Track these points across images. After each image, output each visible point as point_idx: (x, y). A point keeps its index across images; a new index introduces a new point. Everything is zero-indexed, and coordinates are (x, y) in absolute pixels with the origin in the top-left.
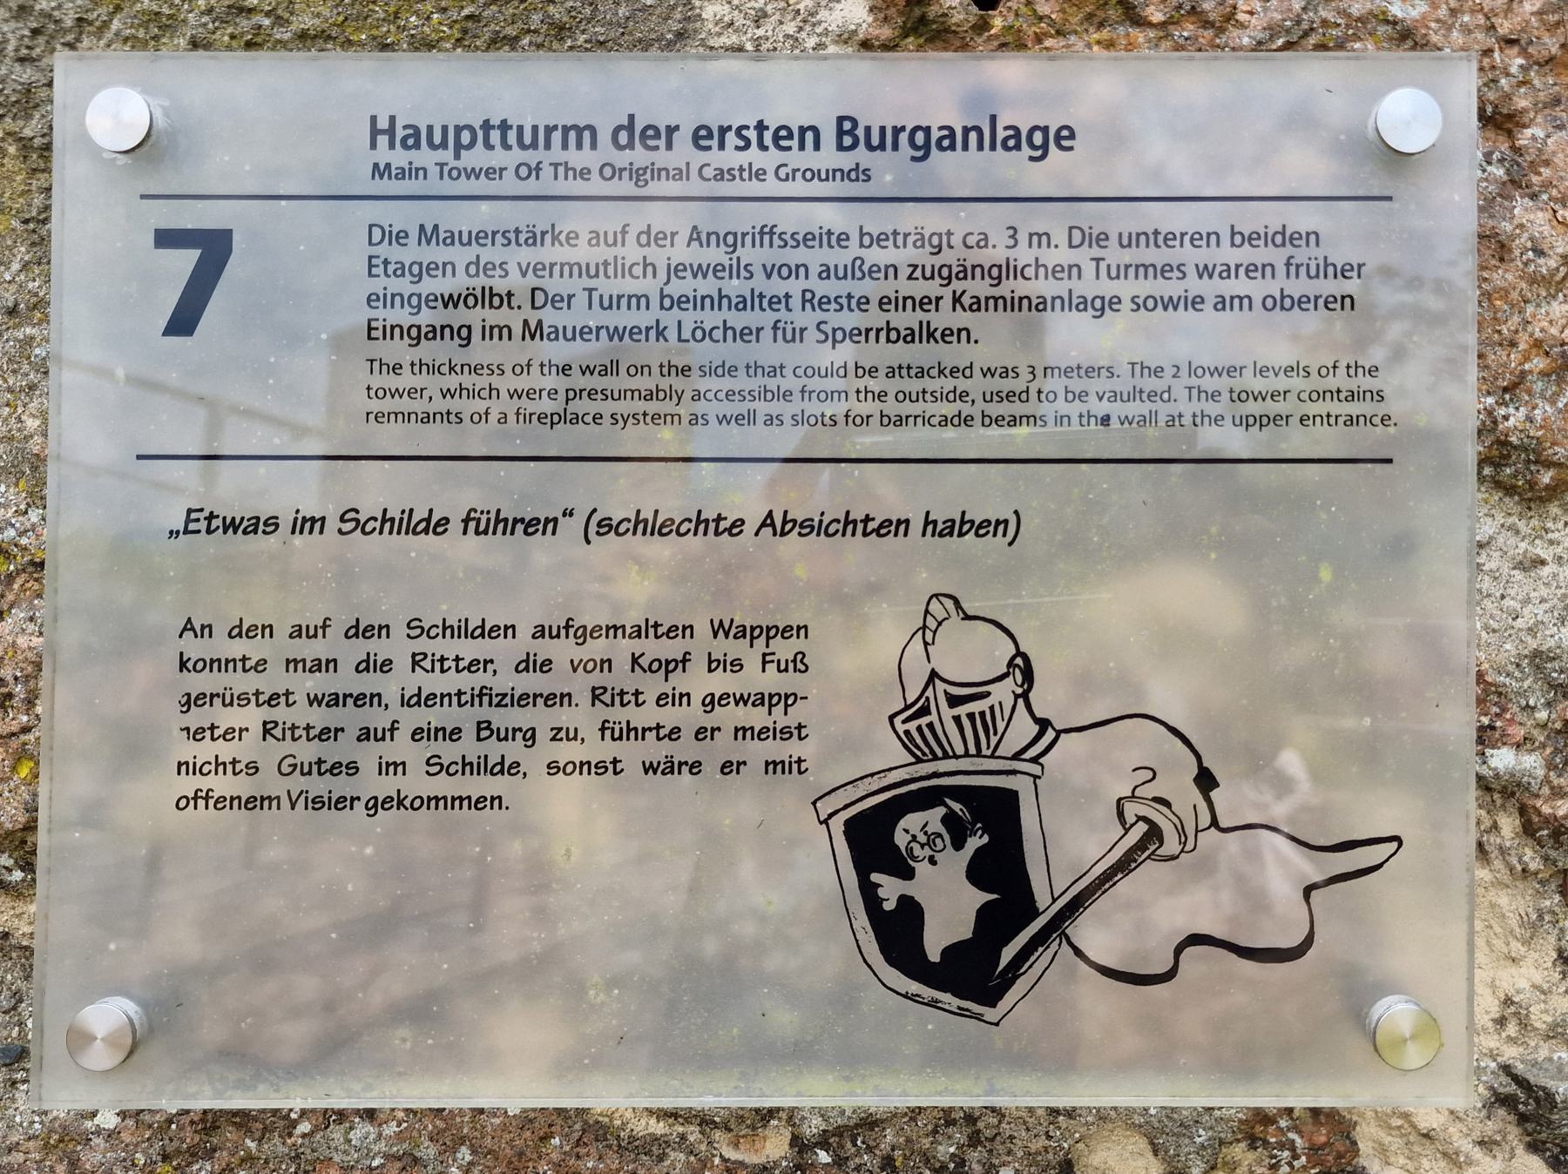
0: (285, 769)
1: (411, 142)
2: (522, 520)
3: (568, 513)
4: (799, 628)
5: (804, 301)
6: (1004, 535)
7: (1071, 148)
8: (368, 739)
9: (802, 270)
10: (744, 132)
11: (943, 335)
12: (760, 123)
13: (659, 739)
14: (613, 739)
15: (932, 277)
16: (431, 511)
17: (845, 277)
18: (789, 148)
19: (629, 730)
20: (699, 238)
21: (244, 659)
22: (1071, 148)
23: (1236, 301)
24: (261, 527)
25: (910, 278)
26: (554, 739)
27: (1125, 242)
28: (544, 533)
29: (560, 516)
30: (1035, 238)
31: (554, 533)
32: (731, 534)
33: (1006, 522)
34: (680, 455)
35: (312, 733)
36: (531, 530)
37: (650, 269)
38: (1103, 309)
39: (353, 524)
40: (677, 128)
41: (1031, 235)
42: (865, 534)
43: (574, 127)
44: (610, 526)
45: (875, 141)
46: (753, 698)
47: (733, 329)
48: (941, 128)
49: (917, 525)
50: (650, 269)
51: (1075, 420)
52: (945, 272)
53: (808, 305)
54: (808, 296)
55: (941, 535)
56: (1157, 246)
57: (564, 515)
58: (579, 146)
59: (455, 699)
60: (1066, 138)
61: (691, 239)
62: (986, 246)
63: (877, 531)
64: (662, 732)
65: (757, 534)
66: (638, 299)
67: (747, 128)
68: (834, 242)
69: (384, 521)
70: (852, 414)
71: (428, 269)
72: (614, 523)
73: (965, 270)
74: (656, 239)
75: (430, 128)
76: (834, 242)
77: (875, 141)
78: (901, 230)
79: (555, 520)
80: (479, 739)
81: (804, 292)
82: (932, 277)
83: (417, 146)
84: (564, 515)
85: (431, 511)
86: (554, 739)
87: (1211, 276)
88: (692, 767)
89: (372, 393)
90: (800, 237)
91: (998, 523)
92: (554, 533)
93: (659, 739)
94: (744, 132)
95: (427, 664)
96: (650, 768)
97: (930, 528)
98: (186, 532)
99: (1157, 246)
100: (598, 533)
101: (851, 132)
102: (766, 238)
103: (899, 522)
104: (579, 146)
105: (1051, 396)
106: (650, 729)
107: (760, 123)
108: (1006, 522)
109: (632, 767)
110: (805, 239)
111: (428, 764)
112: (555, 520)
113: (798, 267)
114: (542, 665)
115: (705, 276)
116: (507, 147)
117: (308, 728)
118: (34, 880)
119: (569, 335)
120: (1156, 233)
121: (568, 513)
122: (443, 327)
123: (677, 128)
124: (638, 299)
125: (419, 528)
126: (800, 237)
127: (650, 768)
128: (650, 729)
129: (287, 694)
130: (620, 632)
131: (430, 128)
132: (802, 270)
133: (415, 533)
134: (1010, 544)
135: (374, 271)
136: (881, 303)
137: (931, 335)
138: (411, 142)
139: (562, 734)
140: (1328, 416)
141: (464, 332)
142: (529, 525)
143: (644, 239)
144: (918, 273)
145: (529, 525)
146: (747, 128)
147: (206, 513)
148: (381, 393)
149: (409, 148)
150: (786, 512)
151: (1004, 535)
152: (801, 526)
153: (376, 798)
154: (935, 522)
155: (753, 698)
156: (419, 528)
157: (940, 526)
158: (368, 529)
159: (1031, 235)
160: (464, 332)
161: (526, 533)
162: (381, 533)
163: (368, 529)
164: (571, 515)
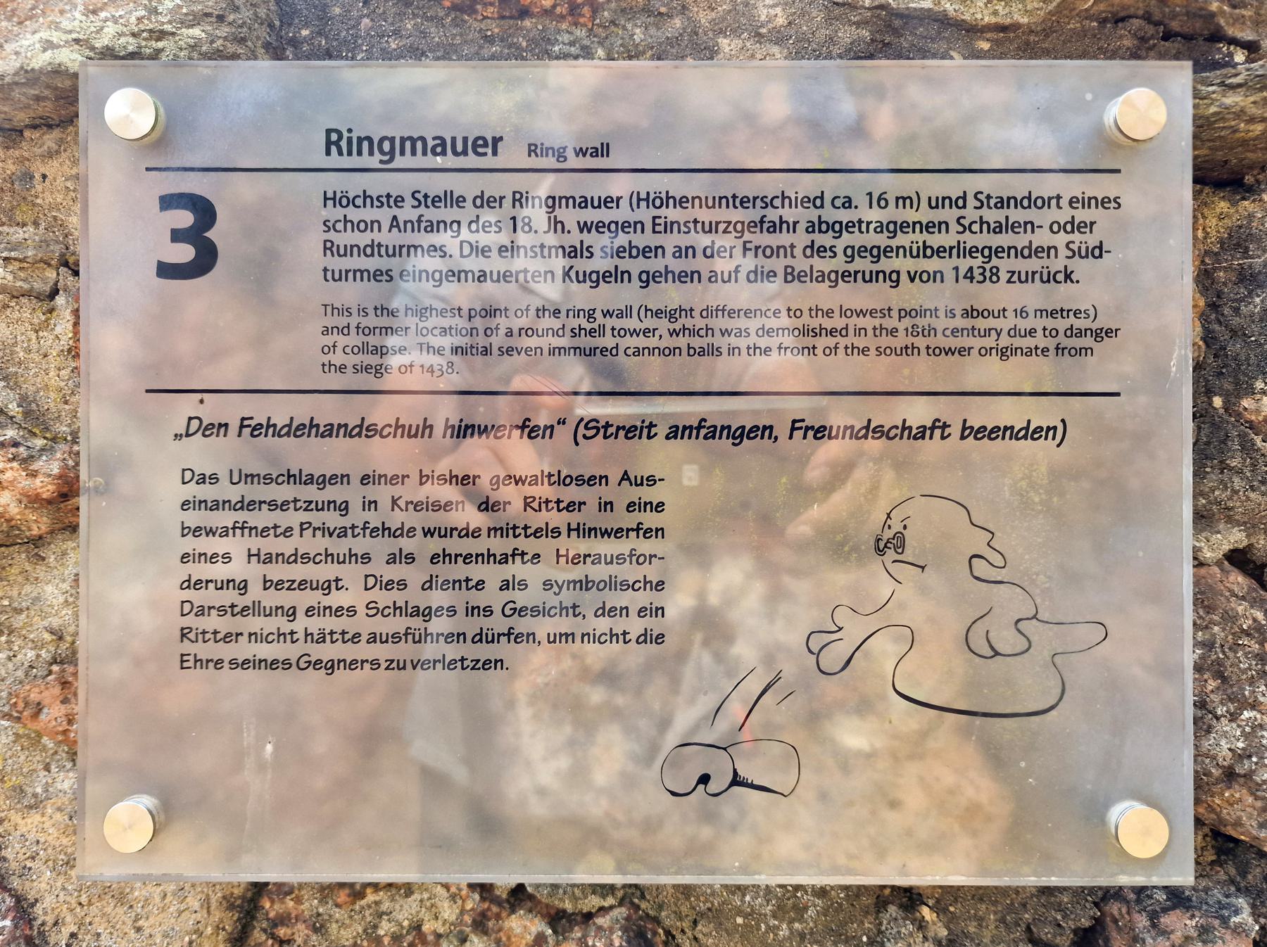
0: (508, 612)
1: (439, 150)
2: (624, 428)
3: (562, 422)
4: (657, 530)
5: (514, 200)
6: (1054, 439)
8: (375, 641)
9: (376, 225)
14: (414, 642)
15: (584, 281)
16: (363, 419)
17: (918, 256)
18: (485, 154)
19: (426, 635)
20: (398, 226)
21: (467, 580)
24: (364, 432)
25: (1009, 281)
27: (626, 275)
28: (1046, 439)
30: (901, 201)
31: (551, 437)
33: (1055, 428)
34: (1023, 398)
35: (219, 636)
36: (256, 433)
38: (879, 256)
39: (594, 431)
40: (501, 138)
41: (897, 199)
43: (410, 138)
44: (376, 430)
45: (365, 144)
47: (673, 273)
48: (434, 139)
51: (870, 332)
52: (891, 227)
53: (328, 252)
54: (518, 196)
55: (322, 436)
56: (735, 207)
58: (414, 153)
59: (464, 584)
60: (481, 146)
61: (392, 226)
62: (850, 207)
65: (791, 437)
68: (738, 204)
69: (397, 427)
70: (362, 326)
71: (901, 227)
74: (488, 201)
75: (454, 139)
76: (738, 204)
77: (365, 144)
78: (865, 219)
79: (552, 427)
80: (786, 281)
81: (786, 267)
82: (584, 281)
83: (444, 153)
85: (363, 419)
88: (216, 663)
91: (1049, 429)
92: (551, 437)
95: (192, 636)
97: (906, 432)
98: (188, 435)
99: (735, 207)
100: (585, 437)
101: (791, 274)
103: (220, 425)
104: (414, 153)
105: (798, 313)
108: (1055, 428)
112: (552, 427)
113: (372, 222)
114: (657, 638)
115: (589, 231)
117: (215, 633)
118: (754, 886)
119: (596, 204)
120: (734, 197)
122: (438, 222)
123: (501, 138)
131: (454, 139)
132: (376, 225)
133: (351, 436)
134: (1058, 446)
135: (657, 229)
136: (1071, 202)
138: (439, 150)
140: (734, 197)
141: (894, 277)
142: (629, 431)
143: (478, 202)
144: (1015, 278)
145: (629, 431)
147: (602, 423)
148: (622, 333)
149: (438, 154)
150: (965, 421)
151: (1054, 439)
154: (910, 428)
157: (914, 431)
158: (385, 433)
159: (897, 199)
160: (894, 277)
161: (626, 437)
162: (901, 438)
163: (385, 433)
164: (564, 423)
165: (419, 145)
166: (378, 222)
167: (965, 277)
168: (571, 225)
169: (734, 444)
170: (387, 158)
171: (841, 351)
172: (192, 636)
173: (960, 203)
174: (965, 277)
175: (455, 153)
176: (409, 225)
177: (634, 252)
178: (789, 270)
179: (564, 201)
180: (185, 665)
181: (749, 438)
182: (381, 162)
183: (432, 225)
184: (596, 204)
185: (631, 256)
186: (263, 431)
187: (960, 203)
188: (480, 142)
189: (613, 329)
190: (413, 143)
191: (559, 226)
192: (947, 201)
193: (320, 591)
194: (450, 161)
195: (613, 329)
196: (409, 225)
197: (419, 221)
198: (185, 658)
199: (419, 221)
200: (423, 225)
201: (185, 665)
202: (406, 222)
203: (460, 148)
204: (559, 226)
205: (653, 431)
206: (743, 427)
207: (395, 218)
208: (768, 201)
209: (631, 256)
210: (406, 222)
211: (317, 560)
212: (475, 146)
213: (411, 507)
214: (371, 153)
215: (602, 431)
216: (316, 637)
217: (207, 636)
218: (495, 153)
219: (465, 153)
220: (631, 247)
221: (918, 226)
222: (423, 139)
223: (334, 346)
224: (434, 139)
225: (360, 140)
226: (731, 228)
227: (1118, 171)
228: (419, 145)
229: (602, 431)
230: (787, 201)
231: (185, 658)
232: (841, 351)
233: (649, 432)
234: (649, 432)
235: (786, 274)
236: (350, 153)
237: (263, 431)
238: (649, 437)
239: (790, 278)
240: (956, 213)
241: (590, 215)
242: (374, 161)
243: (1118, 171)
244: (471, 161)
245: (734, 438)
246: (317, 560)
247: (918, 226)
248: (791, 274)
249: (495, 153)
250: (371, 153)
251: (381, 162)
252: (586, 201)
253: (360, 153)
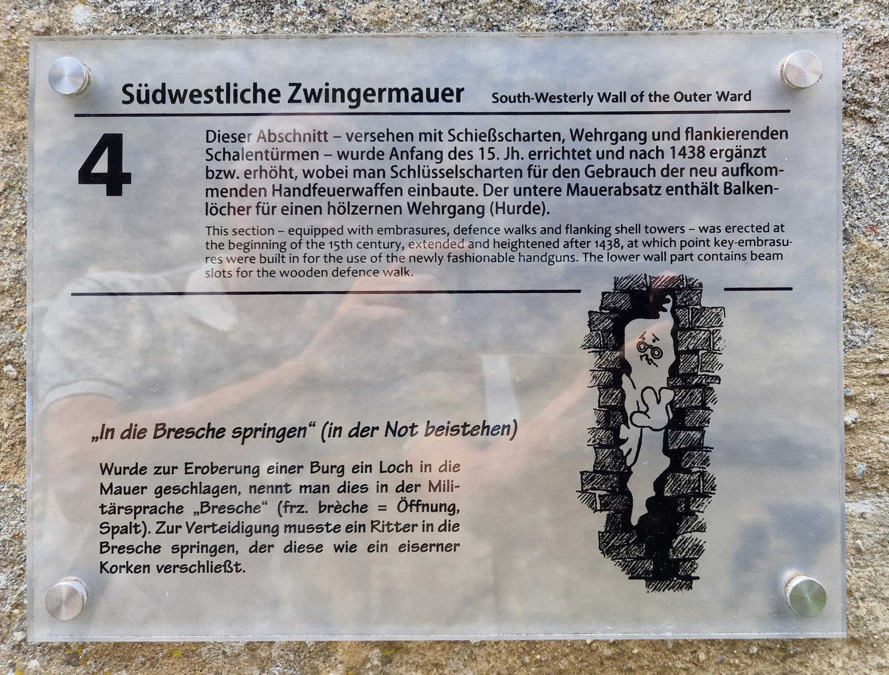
3: (312, 425)
6: (508, 434)
7: (278, 102)
10: (209, 93)
11: (757, 189)
12: (219, 87)
13: (214, 532)
16: (359, 423)
18: (451, 101)
20: (396, 155)
22: (278, 102)
23: (768, 170)
26: (156, 473)
29: (307, 426)
30: (210, 192)
31: (112, 438)
32: (472, 435)
33: (509, 426)
36: (179, 435)
37: (652, 171)
40: (463, 89)
42: (464, 434)
43: (396, 89)
44: (193, 432)
45: (339, 94)
46: (365, 190)
48: (414, 89)
49: (421, 429)
50: (652, 171)
57: (310, 425)
59: (284, 489)
61: (392, 155)
63: (471, 432)
64: (216, 528)
66: (360, 171)
67: (211, 90)
68: (465, 193)
69: (209, 430)
72: (196, 431)
73: (741, 152)
74: (772, 134)
76: (537, 193)
79: (305, 428)
81: (725, 183)
83: (421, 100)
84: (310, 425)
85: (359, 423)
86: (156, 473)
87: (361, 195)
89: (648, 230)
90: (444, 172)
91: (504, 427)
93: (214, 532)
94: (209, 93)
95: (380, 527)
96: (338, 549)
102: (379, 190)
104: (399, 100)
106: (209, 526)
107: (219, 87)
108: (509, 426)
109: (328, 548)
110: (447, 173)
111: (101, 527)
112: (305, 428)
116: (220, 101)
117: (397, 524)
121: (312, 425)
123: (463, 89)
124: (360, 171)
125: (249, 432)
126: (444, 172)
127: (338, 549)
128: (209, 526)
129: (287, 485)
130: (308, 489)
131: (428, 90)
134: (511, 439)
137: (750, 189)
138: (417, 98)
139: (161, 470)
142: (178, 432)
143: (557, 173)
145: (178, 432)
146: (211, 90)
148: (653, 230)
151: (508, 434)
152: (187, 433)
153: (215, 546)
155: (365, 190)
156: (249, 432)
158: (199, 435)
159: (207, 190)
160: (642, 136)
161: (176, 437)
162: (207, 437)
163: (199, 435)
164: (314, 425)
165: (403, 94)
166: (320, 207)
167: (680, 154)
168: (524, 153)
169: (277, 441)
170: (354, 104)
171: (384, 259)
172: (380, 527)
173: (676, 136)
174: (680, 154)
175: (429, 100)
176: (405, 154)
177: (610, 173)
178: (728, 185)
179: (768, 170)
180: (189, 471)
181: (288, 437)
182: (351, 107)
183: (421, 154)
184: (594, 192)
185: (607, 176)
186: (480, 431)
187: (676, 136)
188: (448, 92)
189: (646, 227)
190: (368, 94)
191: (515, 154)
192: (633, 135)
193: (212, 494)
194: (426, 106)
195: (646, 227)
196: (405, 154)
197: (412, 151)
198: (189, 466)
199: (412, 151)
200: (415, 154)
201: (189, 471)
202: (402, 152)
203: (432, 97)
204: (515, 154)
205: (415, 430)
206: (284, 429)
207: (394, 149)
208: (503, 135)
209: (607, 176)
210: (402, 152)
211: (239, 510)
212: (444, 95)
213: (199, 471)
214: (343, 100)
215: (410, 430)
216: (313, 489)
217: (391, 527)
218: (458, 100)
219: (436, 100)
220: (607, 169)
221: (755, 134)
222: (405, 90)
223: (380, 256)
224: (414, 89)
225: (335, 91)
226: (216, 173)
227: (788, 111)
228: (403, 94)
229: (410, 430)
230: (469, 136)
231: (189, 466)
232: (384, 259)
233: (412, 431)
234: (412, 431)
235: (725, 188)
236: (228, 101)
237: (444, 431)
238: (412, 435)
239: (728, 191)
240: (672, 143)
241: (537, 145)
242: (345, 106)
243: (788, 111)
244: (441, 106)
245: (278, 437)
246: (239, 510)
247: (755, 134)
248: (729, 188)
249: (458, 100)
250: (343, 100)
251: (351, 107)
252: (447, 191)
253: (334, 100)
